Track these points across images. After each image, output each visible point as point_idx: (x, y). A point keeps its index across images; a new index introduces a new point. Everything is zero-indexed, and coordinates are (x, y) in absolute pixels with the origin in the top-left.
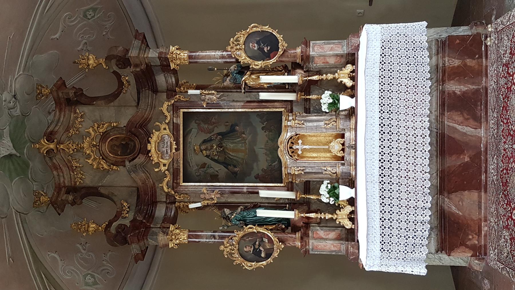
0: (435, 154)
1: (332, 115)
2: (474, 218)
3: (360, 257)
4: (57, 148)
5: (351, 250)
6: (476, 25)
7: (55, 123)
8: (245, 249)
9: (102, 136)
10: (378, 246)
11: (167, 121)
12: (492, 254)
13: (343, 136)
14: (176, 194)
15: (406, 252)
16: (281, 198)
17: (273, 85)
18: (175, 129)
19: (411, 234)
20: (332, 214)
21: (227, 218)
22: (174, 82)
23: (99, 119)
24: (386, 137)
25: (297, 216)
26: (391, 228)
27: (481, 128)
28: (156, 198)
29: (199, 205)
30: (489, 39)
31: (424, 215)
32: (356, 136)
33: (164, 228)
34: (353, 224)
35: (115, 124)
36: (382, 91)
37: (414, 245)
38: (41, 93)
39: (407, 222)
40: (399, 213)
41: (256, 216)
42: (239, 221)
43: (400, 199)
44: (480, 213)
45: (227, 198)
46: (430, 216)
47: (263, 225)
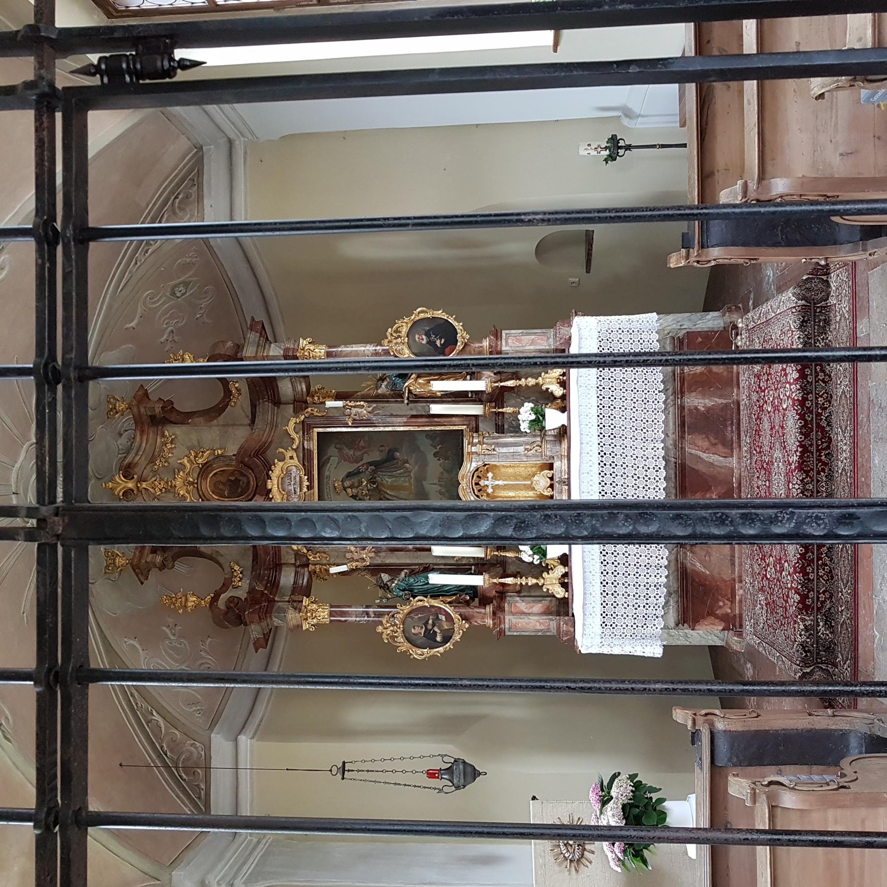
0: (674, 492)
1: (535, 436)
2: (725, 577)
3: (576, 637)
4: (138, 487)
5: (564, 628)
6: (730, 310)
7: (134, 451)
8: (413, 631)
9: (201, 469)
10: (598, 620)
11: (295, 447)
12: (748, 627)
13: (551, 467)
14: (310, 553)
15: (635, 626)
16: (463, 557)
17: (451, 397)
18: (306, 457)
19: (642, 602)
20: (537, 578)
21: (385, 587)
22: (305, 390)
23: (196, 443)
24: (608, 470)
25: (487, 582)
26: (615, 594)
27: (732, 456)
28: (280, 559)
29: (344, 568)
30: (739, 337)
31: (658, 576)
32: (569, 467)
33: (295, 601)
34: (567, 591)
35: (220, 452)
36: (601, 407)
37: (646, 617)
38: (115, 408)
39: (637, 585)
40: (626, 574)
41: (428, 583)
42: (404, 590)
43: (627, 555)
44: (733, 572)
45: (384, 557)
46: (666, 577)
47: (438, 596)
